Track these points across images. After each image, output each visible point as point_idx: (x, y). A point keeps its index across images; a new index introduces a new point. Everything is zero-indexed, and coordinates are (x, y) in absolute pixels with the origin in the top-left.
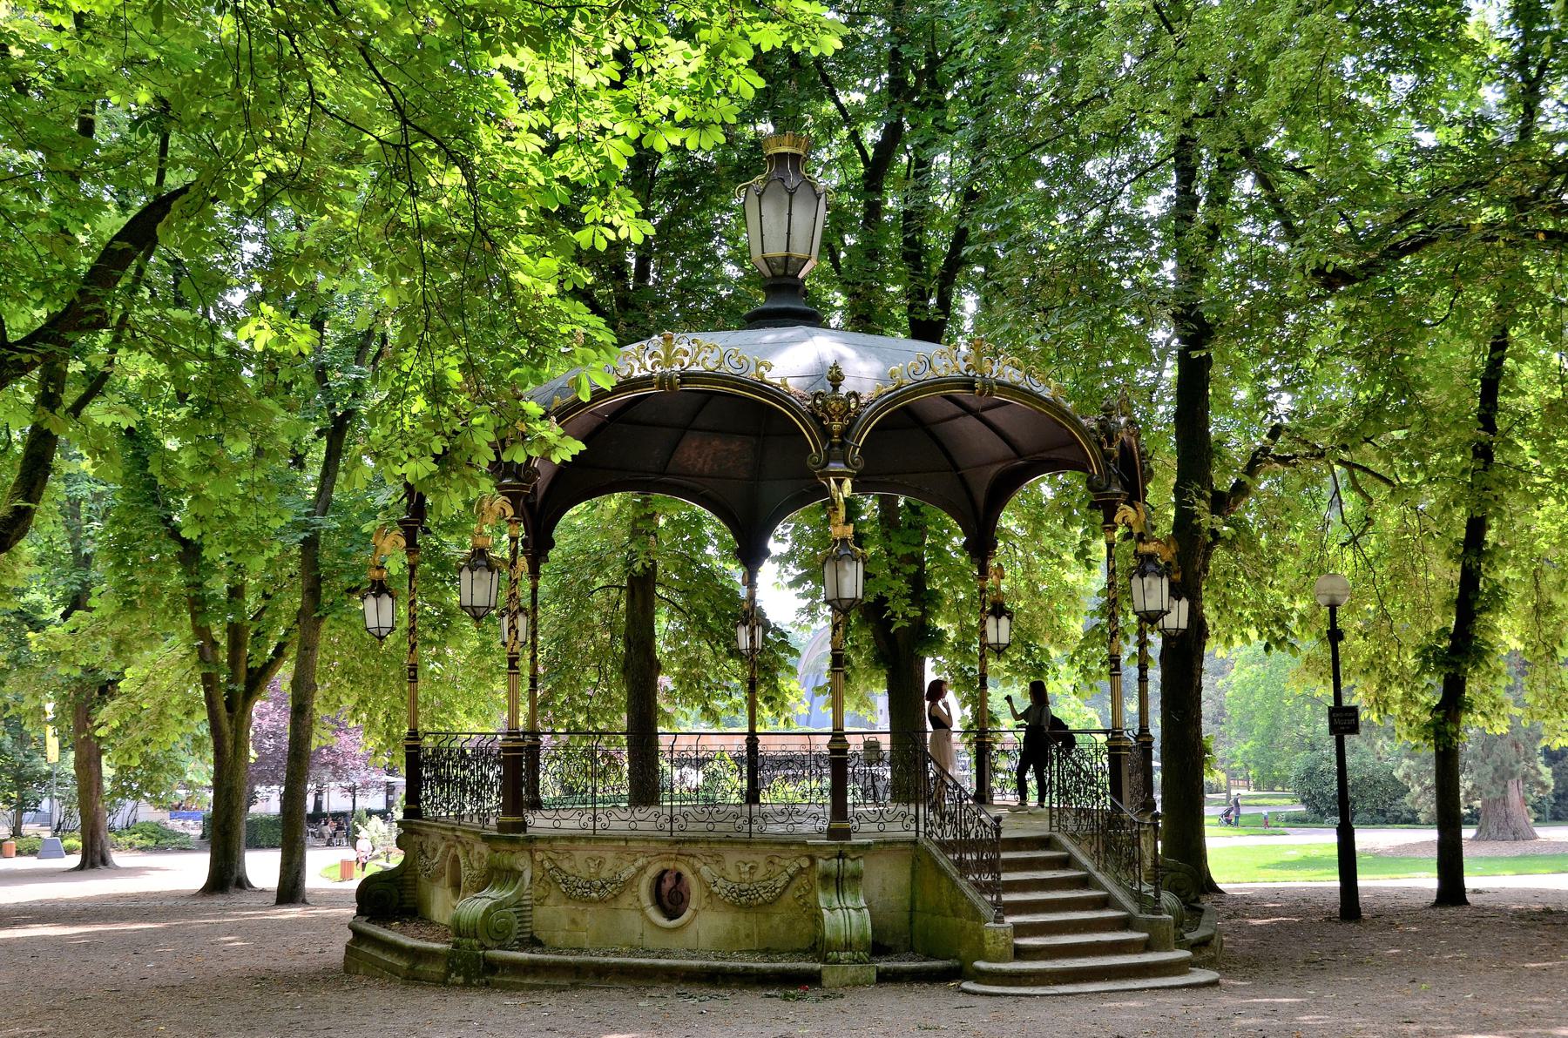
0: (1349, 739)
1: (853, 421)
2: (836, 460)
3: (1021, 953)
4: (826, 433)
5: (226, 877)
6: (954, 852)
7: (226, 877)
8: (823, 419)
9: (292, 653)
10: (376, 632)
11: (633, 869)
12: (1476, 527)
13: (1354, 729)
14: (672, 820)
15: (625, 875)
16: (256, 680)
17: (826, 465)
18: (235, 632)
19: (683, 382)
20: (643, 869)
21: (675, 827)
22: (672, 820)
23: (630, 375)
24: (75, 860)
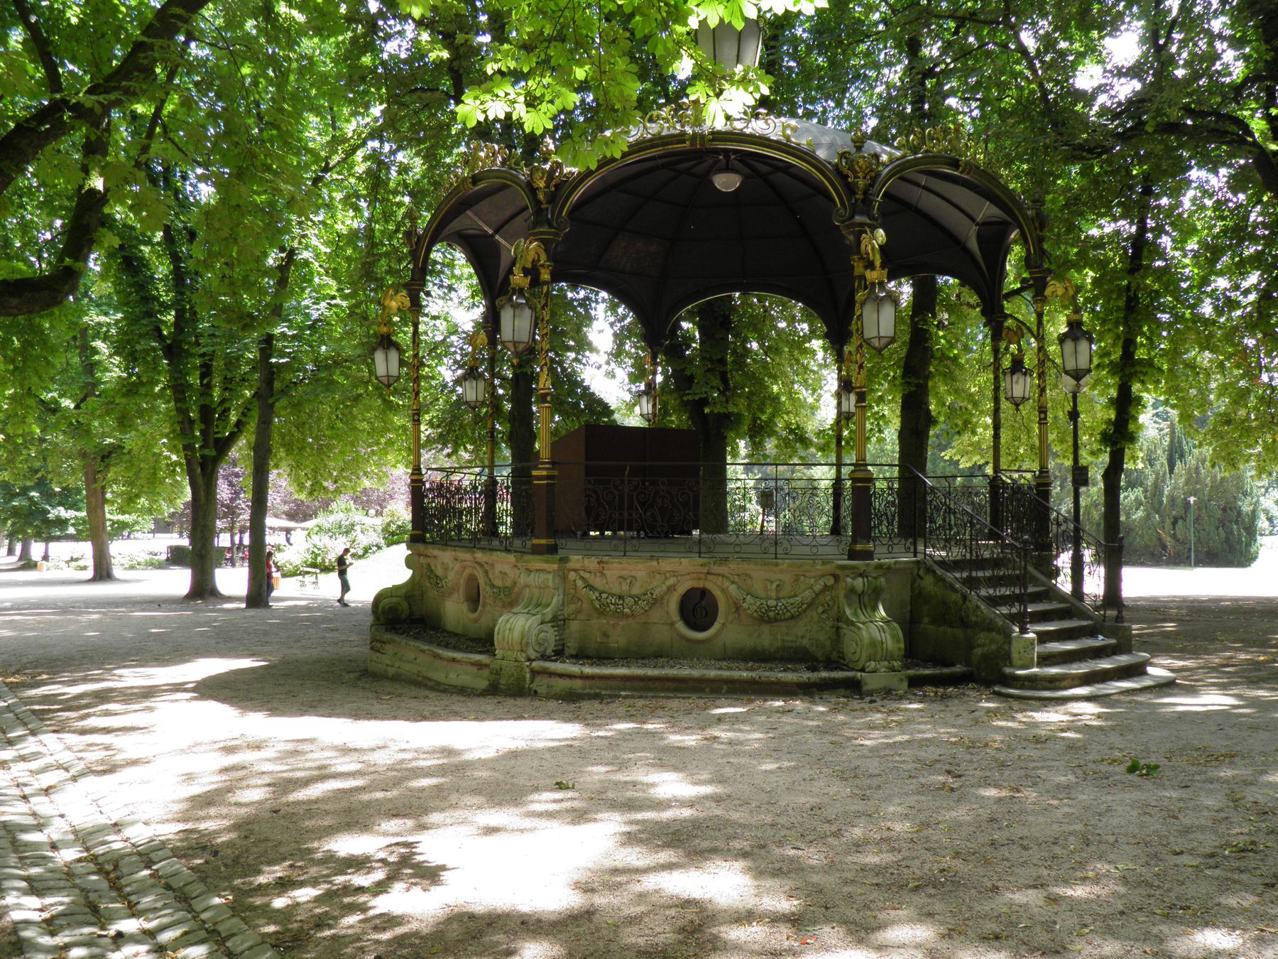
0: (1083, 489)
1: (874, 180)
2: (861, 213)
3: (1046, 660)
4: (850, 189)
5: (203, 590)
6: (962, 570)
7: (203, 590)
8: (847, 176)
9: (252, 426)
10: (385, 380)
11: (664, 588)
12: (1129, 346)
13: (1086, 483)
14: (776, 544)
15: (657, 592)
16: (223, 446)
17: (852, 217)
18: (206, 412)
19: (713, 140)
20: (671, 589)
21: (780, 550)
22: (776, 544)
23: (659, 133)
24: (89, 574)
